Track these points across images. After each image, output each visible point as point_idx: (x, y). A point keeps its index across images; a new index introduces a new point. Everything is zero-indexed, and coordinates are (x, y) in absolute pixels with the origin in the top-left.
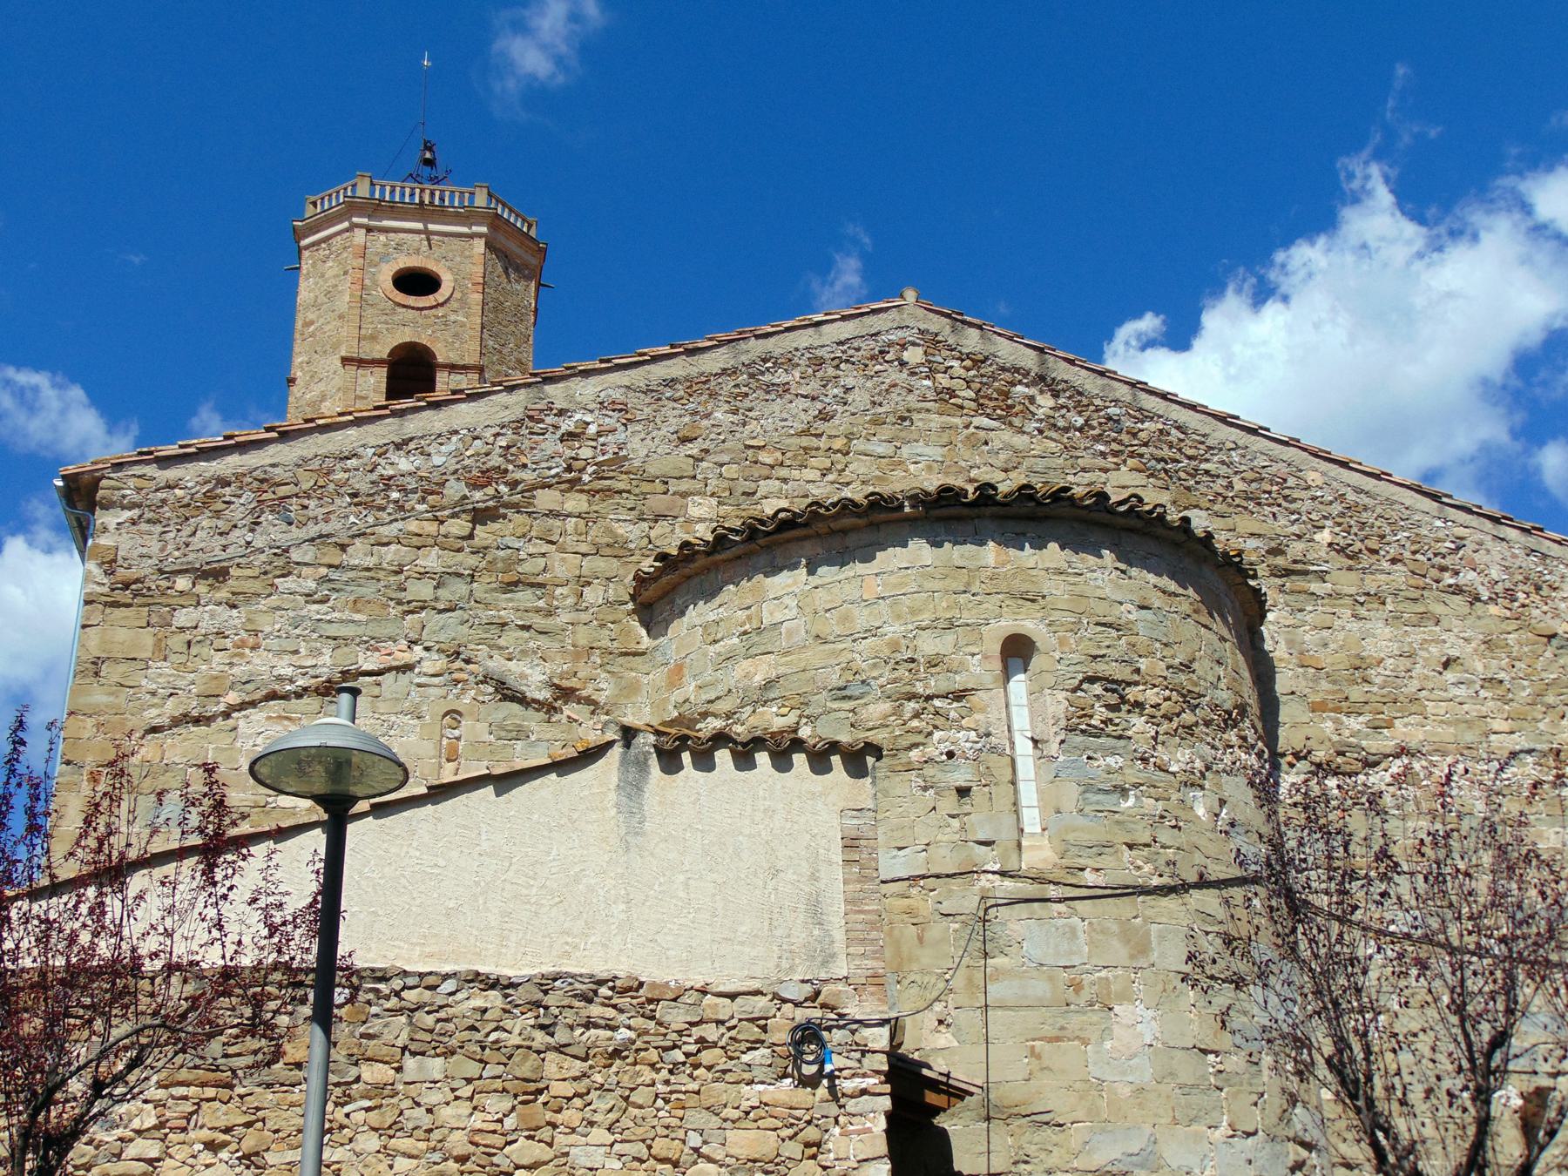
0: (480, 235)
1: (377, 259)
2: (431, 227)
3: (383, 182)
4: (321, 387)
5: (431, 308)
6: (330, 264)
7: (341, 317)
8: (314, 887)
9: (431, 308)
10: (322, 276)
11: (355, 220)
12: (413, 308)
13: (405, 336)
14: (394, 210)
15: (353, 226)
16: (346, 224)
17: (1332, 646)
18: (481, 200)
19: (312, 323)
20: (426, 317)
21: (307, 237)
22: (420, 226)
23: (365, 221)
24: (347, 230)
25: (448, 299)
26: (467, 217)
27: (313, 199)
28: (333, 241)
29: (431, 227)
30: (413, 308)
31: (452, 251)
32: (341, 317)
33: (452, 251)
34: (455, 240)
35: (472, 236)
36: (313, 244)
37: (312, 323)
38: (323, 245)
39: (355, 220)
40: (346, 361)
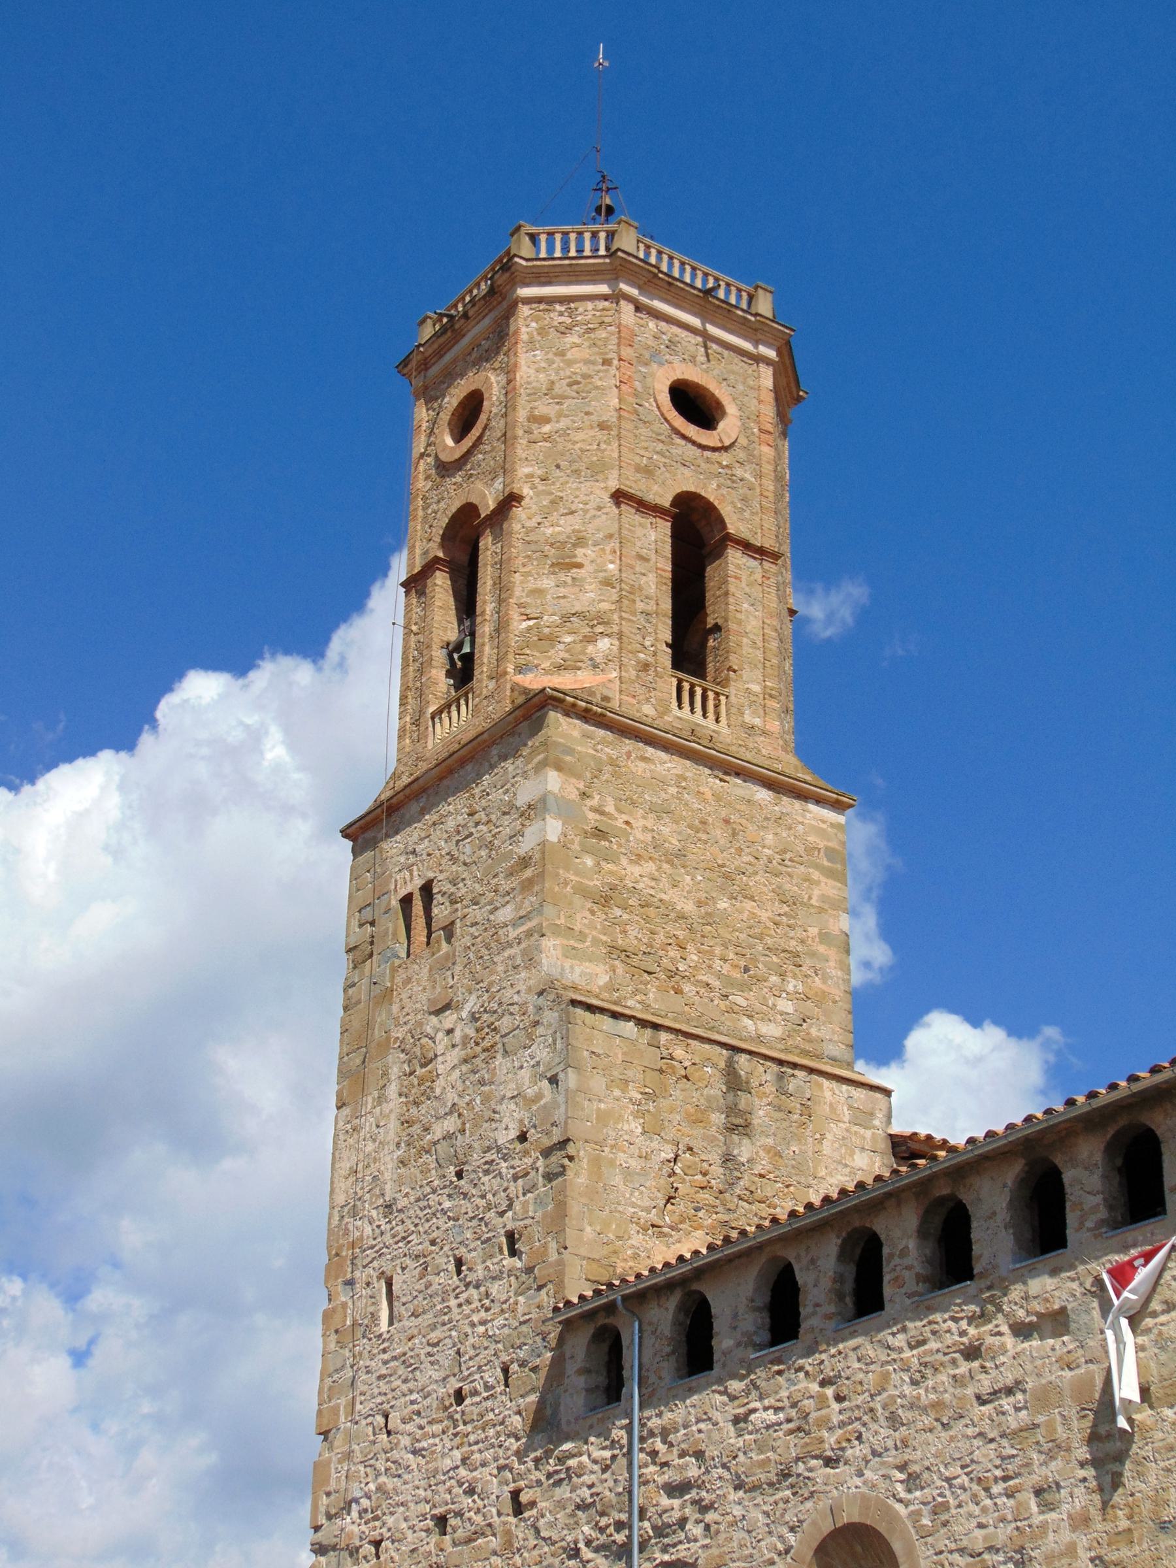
0: (767, 361)
1: (647, 355)
2: (712, 330)
3: (594, 227)
4: (575, 522)
5: (714, 449)
6: (572, 339)
7: (603, 426)
8: (958, 1140)
9: (714, 449)
10: (562, 354)
11: (624, 287)
12: (694, 443)
13: (688, 482)
14: (669, 288)
15: (616, 297)
16: (603, 289)
17: (724, 813)
18: (764, 305)
19: (546, 420)
20: (708, 461)
21: (527, 285)
22: (695, 322)
23: (634, 292)
24: (605, 298)
25: (733, 443)
26: (754, 329)
27: (533, 229)
28: (580, 307)
29: (712, 330)
30: (694, 443)
31: (733, 372)
32: (603, 426)
33: (733, 372)
34: (737, 359)
35: (758, 359)
36: (540, 300)
37: (546, 420)
38: (558, 307)
39: (624, 287)
40: (619, 497)
